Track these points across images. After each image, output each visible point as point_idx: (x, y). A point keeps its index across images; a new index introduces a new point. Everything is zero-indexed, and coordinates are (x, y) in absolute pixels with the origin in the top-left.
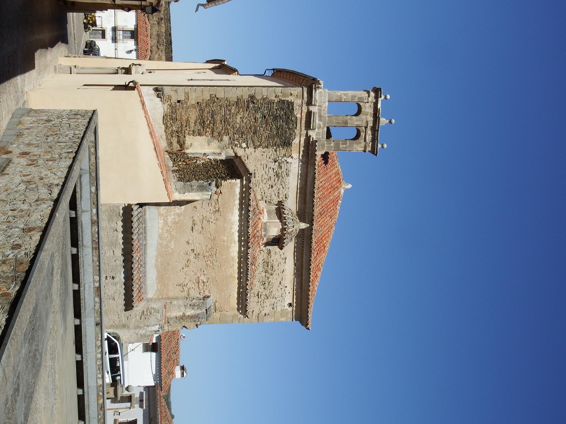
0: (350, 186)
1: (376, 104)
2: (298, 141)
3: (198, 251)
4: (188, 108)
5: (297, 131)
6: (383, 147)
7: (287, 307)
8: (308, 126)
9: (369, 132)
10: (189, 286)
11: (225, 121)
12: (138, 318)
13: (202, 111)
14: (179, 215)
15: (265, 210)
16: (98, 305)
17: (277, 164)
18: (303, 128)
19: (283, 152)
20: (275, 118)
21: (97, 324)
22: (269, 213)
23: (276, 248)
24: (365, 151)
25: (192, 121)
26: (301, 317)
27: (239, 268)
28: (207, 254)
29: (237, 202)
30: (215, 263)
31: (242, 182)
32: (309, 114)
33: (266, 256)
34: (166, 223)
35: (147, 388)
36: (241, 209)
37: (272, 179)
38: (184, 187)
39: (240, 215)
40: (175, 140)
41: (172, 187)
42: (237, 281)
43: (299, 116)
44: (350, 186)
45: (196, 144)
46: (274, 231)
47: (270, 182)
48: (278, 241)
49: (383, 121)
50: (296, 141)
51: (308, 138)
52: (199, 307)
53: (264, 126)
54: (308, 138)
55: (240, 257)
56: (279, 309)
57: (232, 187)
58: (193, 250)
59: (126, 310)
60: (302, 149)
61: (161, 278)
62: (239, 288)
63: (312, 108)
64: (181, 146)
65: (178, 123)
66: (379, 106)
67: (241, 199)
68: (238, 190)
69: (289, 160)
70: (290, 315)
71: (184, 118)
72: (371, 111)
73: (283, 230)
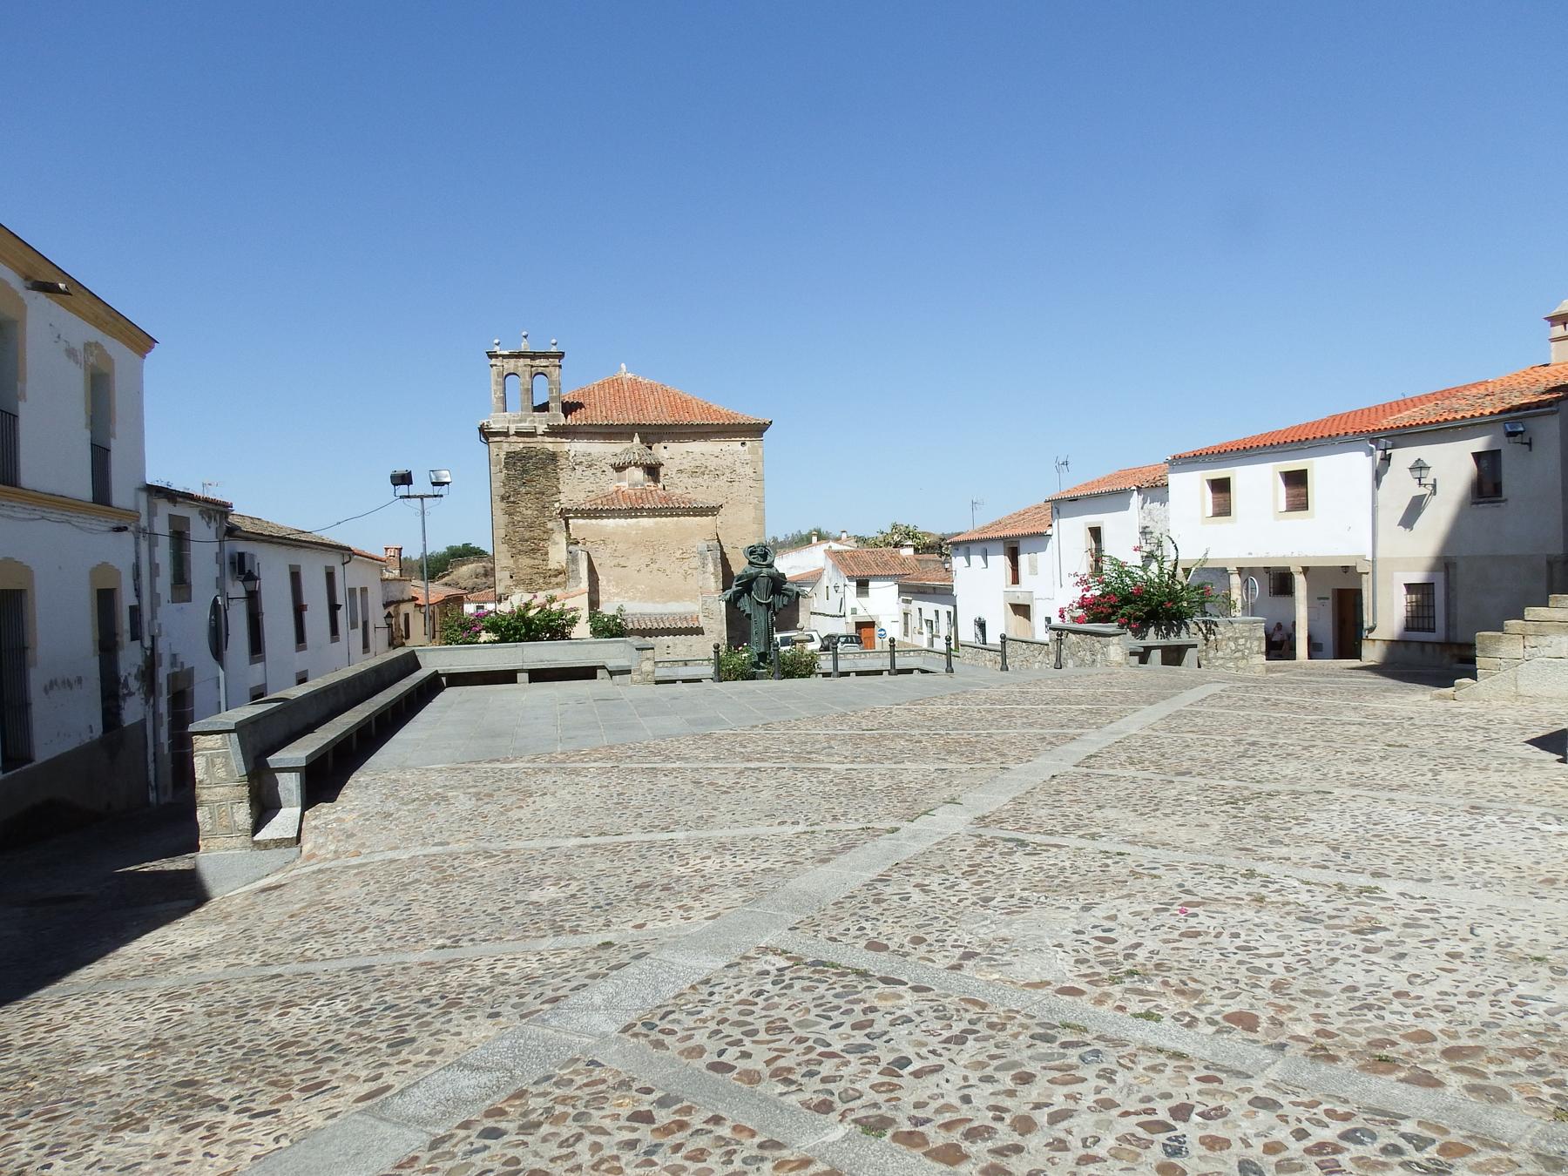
0: (623, 366)
1: (504, 357)
2: (550, 444)
3: (648, 561)
4: (518, 567)
5: (539, 446)
6: (555, 344)
7: (746, 448)
8: (532, 434)
9: (537, 362)
10: (687, 568)
11: (530, 527)
12: (712, 621)
13: (520, 552)
14: (609, 581)
15: (618, 484)
16: (666, 664)
17: (577, 467)
18: (535, 439)
19: (562, 461)
20: (525, 471)
21: (686, 665)
22: (620, 480)
23: (662, 471)
24: (560, 367)
25: (532, 562)
26: (758, 431)
27: (666, 516)
28: (652, 551)
29: (594, 521)
30: (661, 542)
31: (571, 518)
32: (518, 434)
33: (684, 475)
34: (617, 594)
35: (901, 592)
36: (601, 517)
37: (595, 471)
38: (574, 578)
39: (608, 518)
40: (554, 580)
41: (574, 590)
42: (682, 518)
43: (521, 445)
44: (623, 366)
45: (557, 558)
46: (638, 474)
47: (599, 474)
48: (653, 471)
49: (524, 346)
50: (550, 447)
51: (545, 434)
52: (705, 558)
53: (534, 484)
54: (545, 434)
55: (655, 516)
56: (749, 457)
57: (577, 527)
58: (647, 565)
59: (703, 634)
60: (559, 440)
61: (678, 597)
62: (689, 515)
63: (512, 432)
64: (560, 573)
65: (534, 577)
66: (506, 353)
67: (589, 517)
68: (581, 521)
69: (572, 454)
70: (756, 444)
71: (529, 570)
72: (512, 361)
73: (636, 465)
